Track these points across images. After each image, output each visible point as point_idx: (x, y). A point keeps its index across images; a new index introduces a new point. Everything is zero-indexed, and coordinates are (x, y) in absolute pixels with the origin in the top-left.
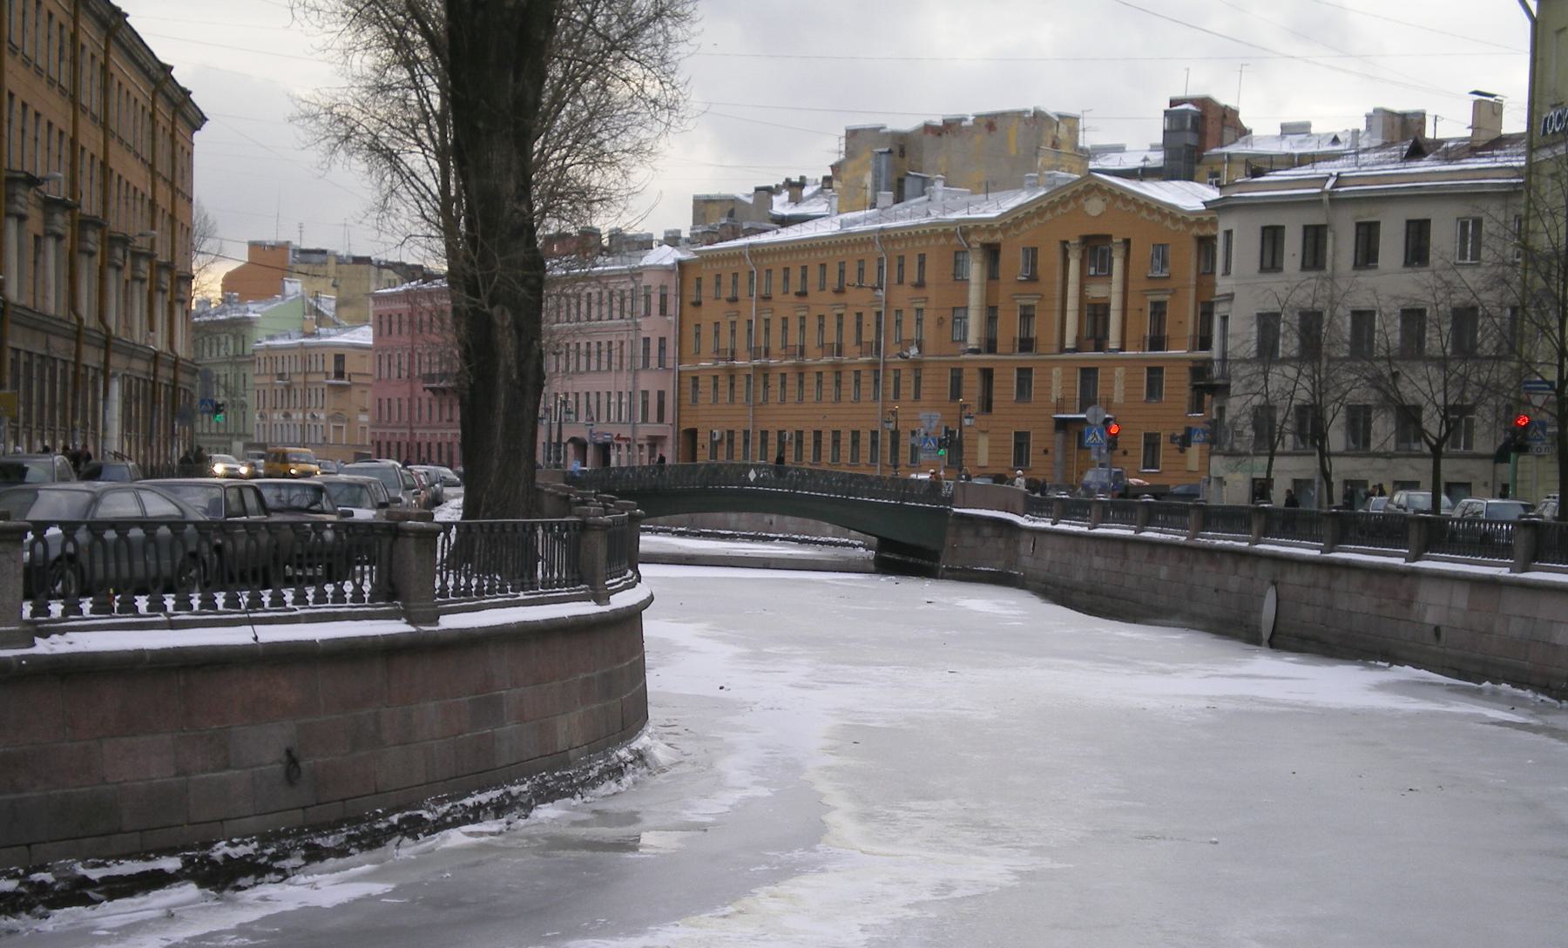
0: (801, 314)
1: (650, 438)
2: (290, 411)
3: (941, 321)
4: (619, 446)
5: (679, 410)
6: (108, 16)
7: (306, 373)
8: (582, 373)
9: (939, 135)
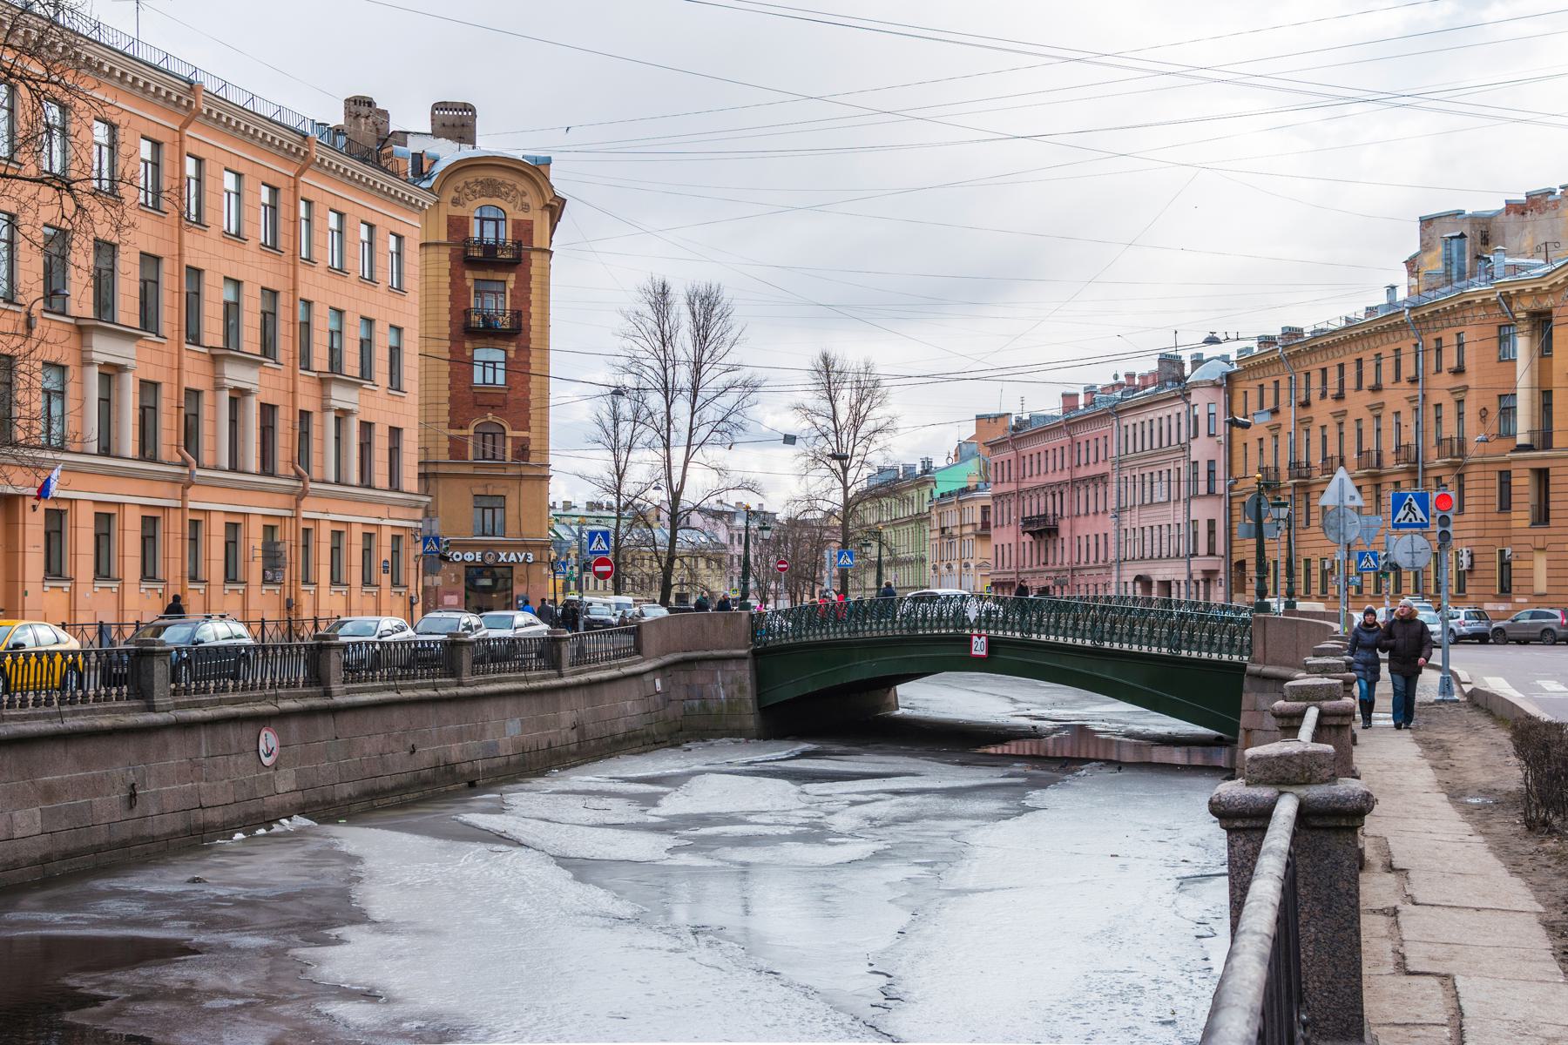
1: (1205, 572)
2: (952, 562)
3: (1484, 414)
7: (961, 526)
9: (1523, 214)
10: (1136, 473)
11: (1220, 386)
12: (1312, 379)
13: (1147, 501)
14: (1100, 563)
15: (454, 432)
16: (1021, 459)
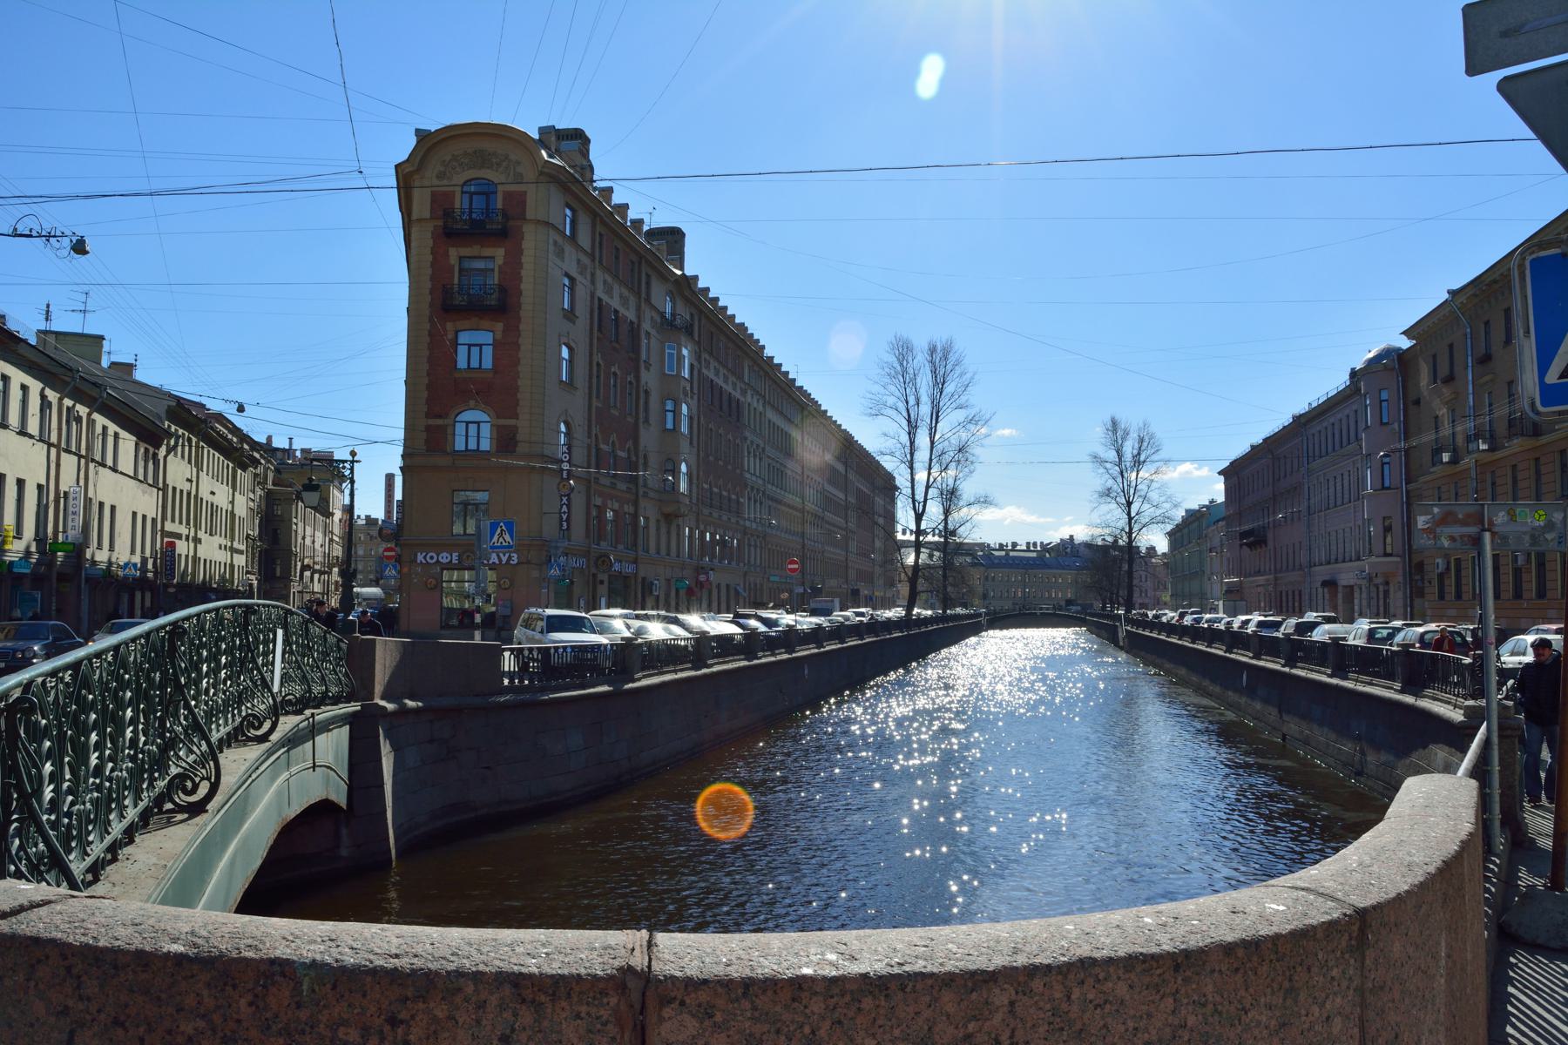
15: (431, 422)
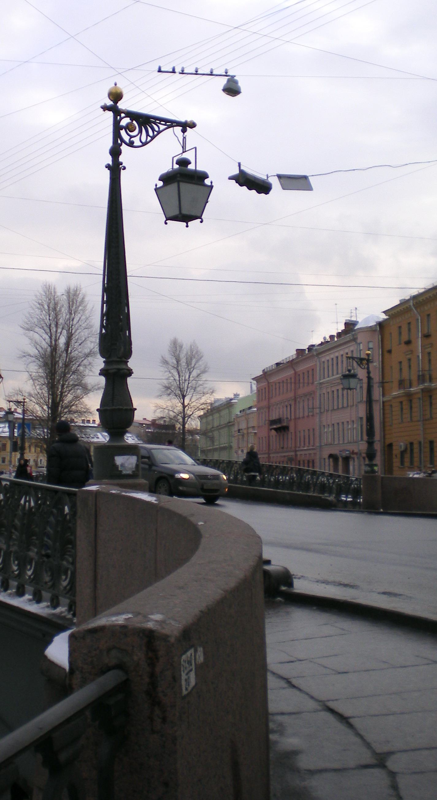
0: (409, 356)
4: (354, 459)
5: (384, 431)
6: (54, 328)
8: (335, 410)
10: (329, 390)
11: (375, 331)
12: (310, 373)
13: (340, 406)
14: (346, 442)
16: (322, 365)
